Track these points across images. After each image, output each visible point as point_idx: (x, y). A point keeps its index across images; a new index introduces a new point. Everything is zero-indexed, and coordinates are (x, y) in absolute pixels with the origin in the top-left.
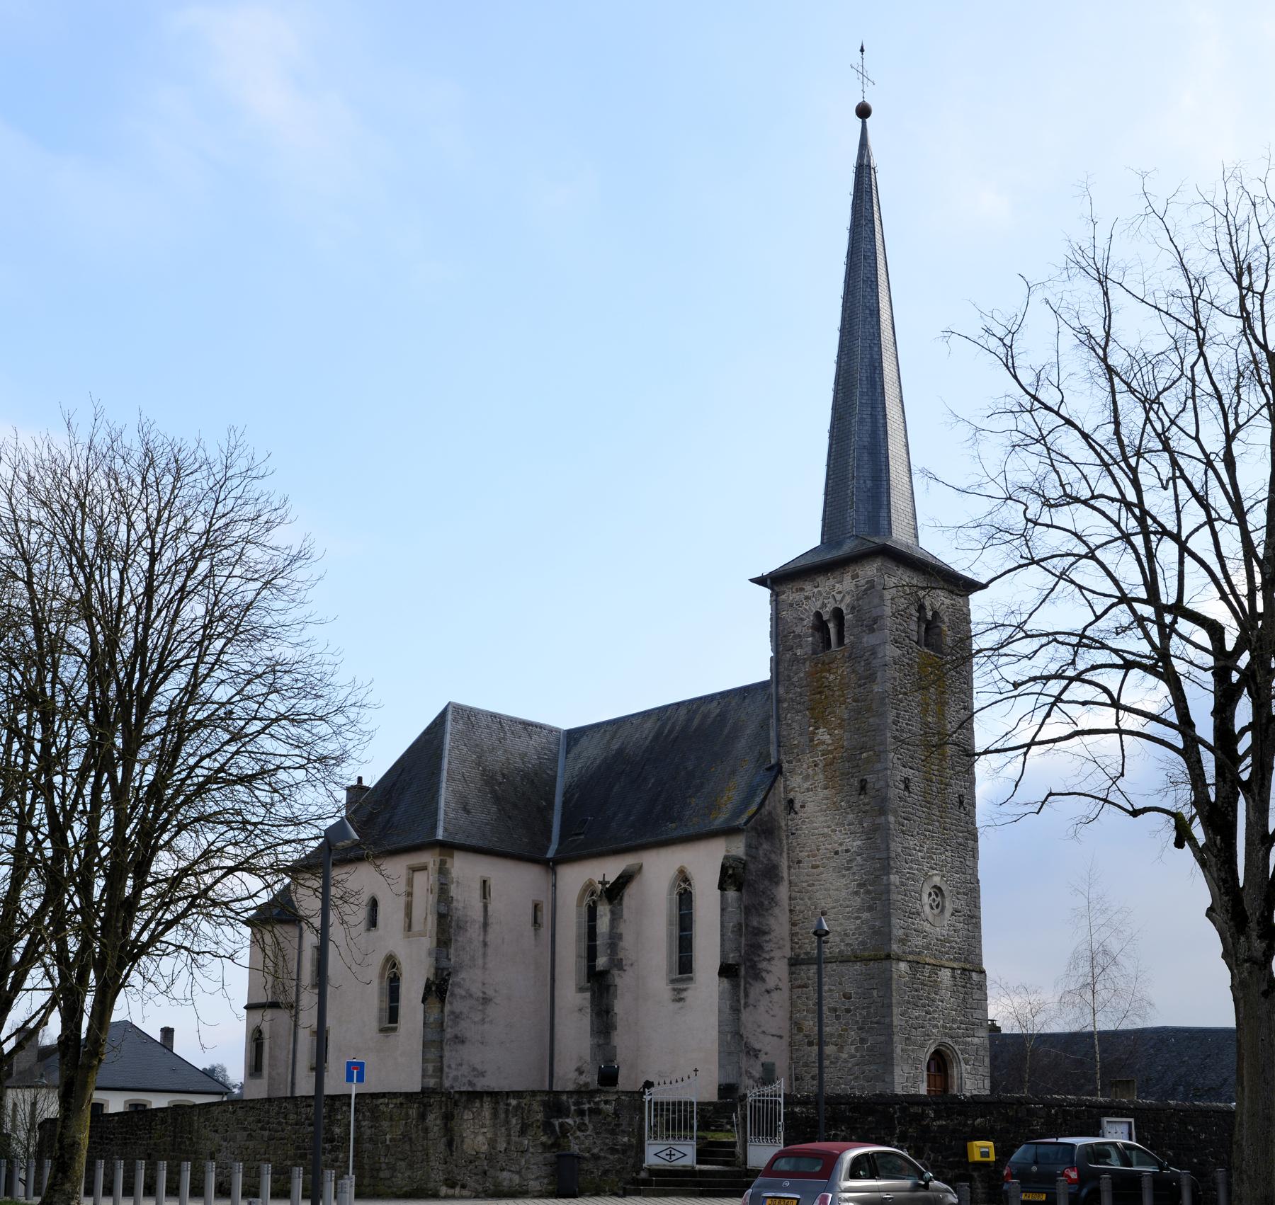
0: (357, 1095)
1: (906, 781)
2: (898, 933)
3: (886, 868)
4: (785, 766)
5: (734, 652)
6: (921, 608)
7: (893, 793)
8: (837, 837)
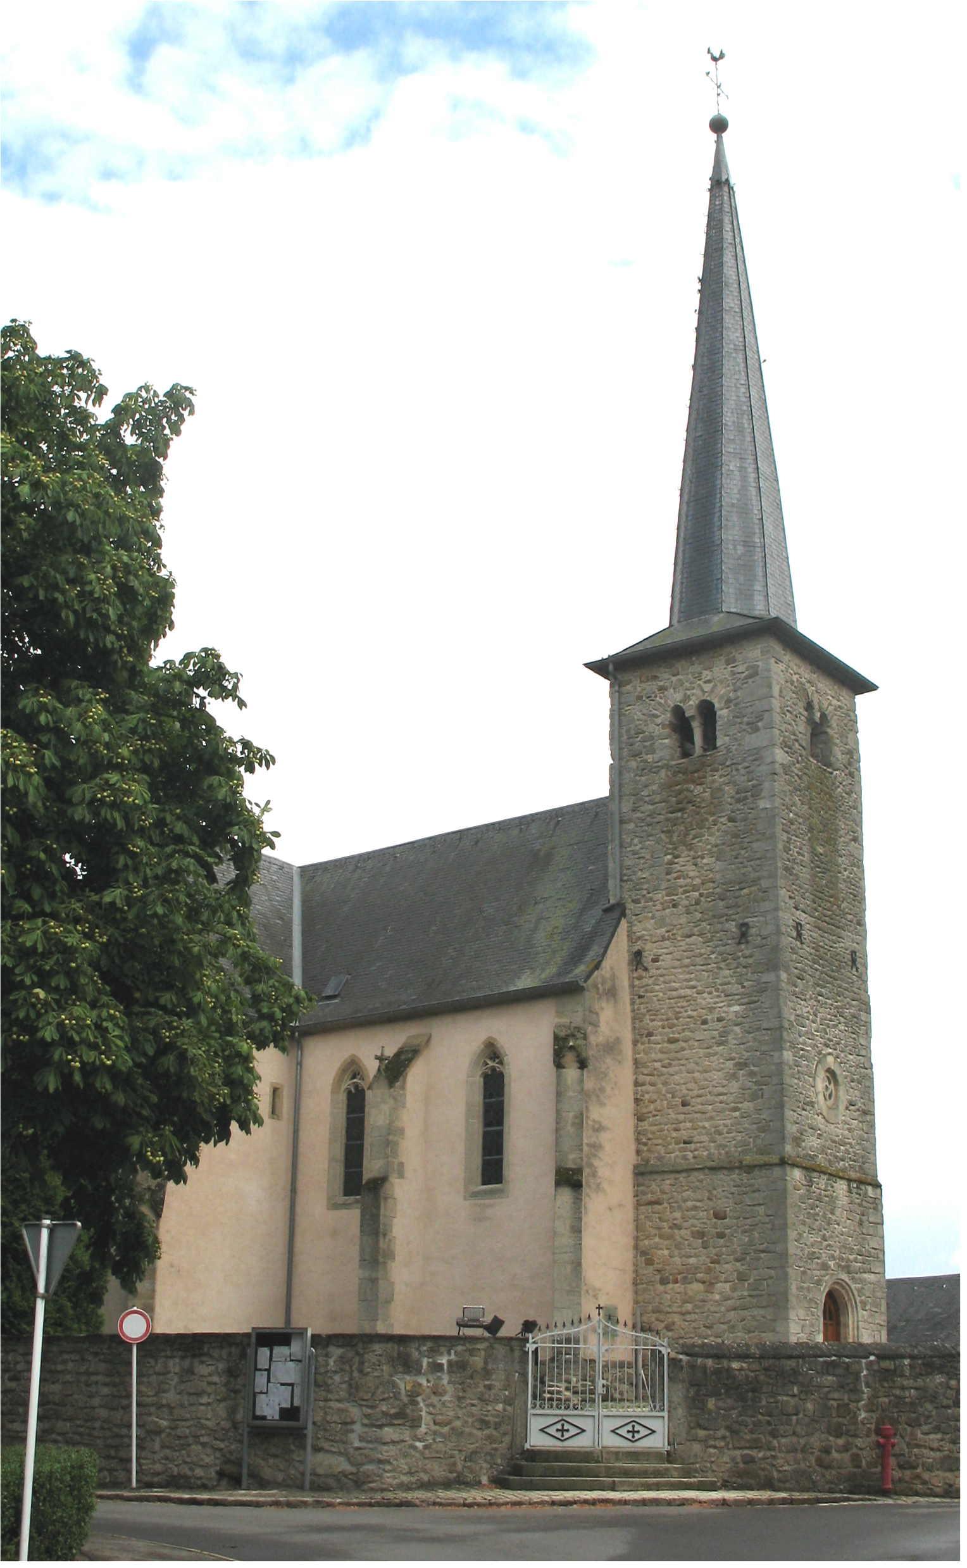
0: (312, 1335)
1: (798, 926)
2: (791, 1129)
3: (778, 1044)
4: (630, 906)
5: (563, 757)
6: (809, 707)
7: (787, 941)
8: (707, 999)
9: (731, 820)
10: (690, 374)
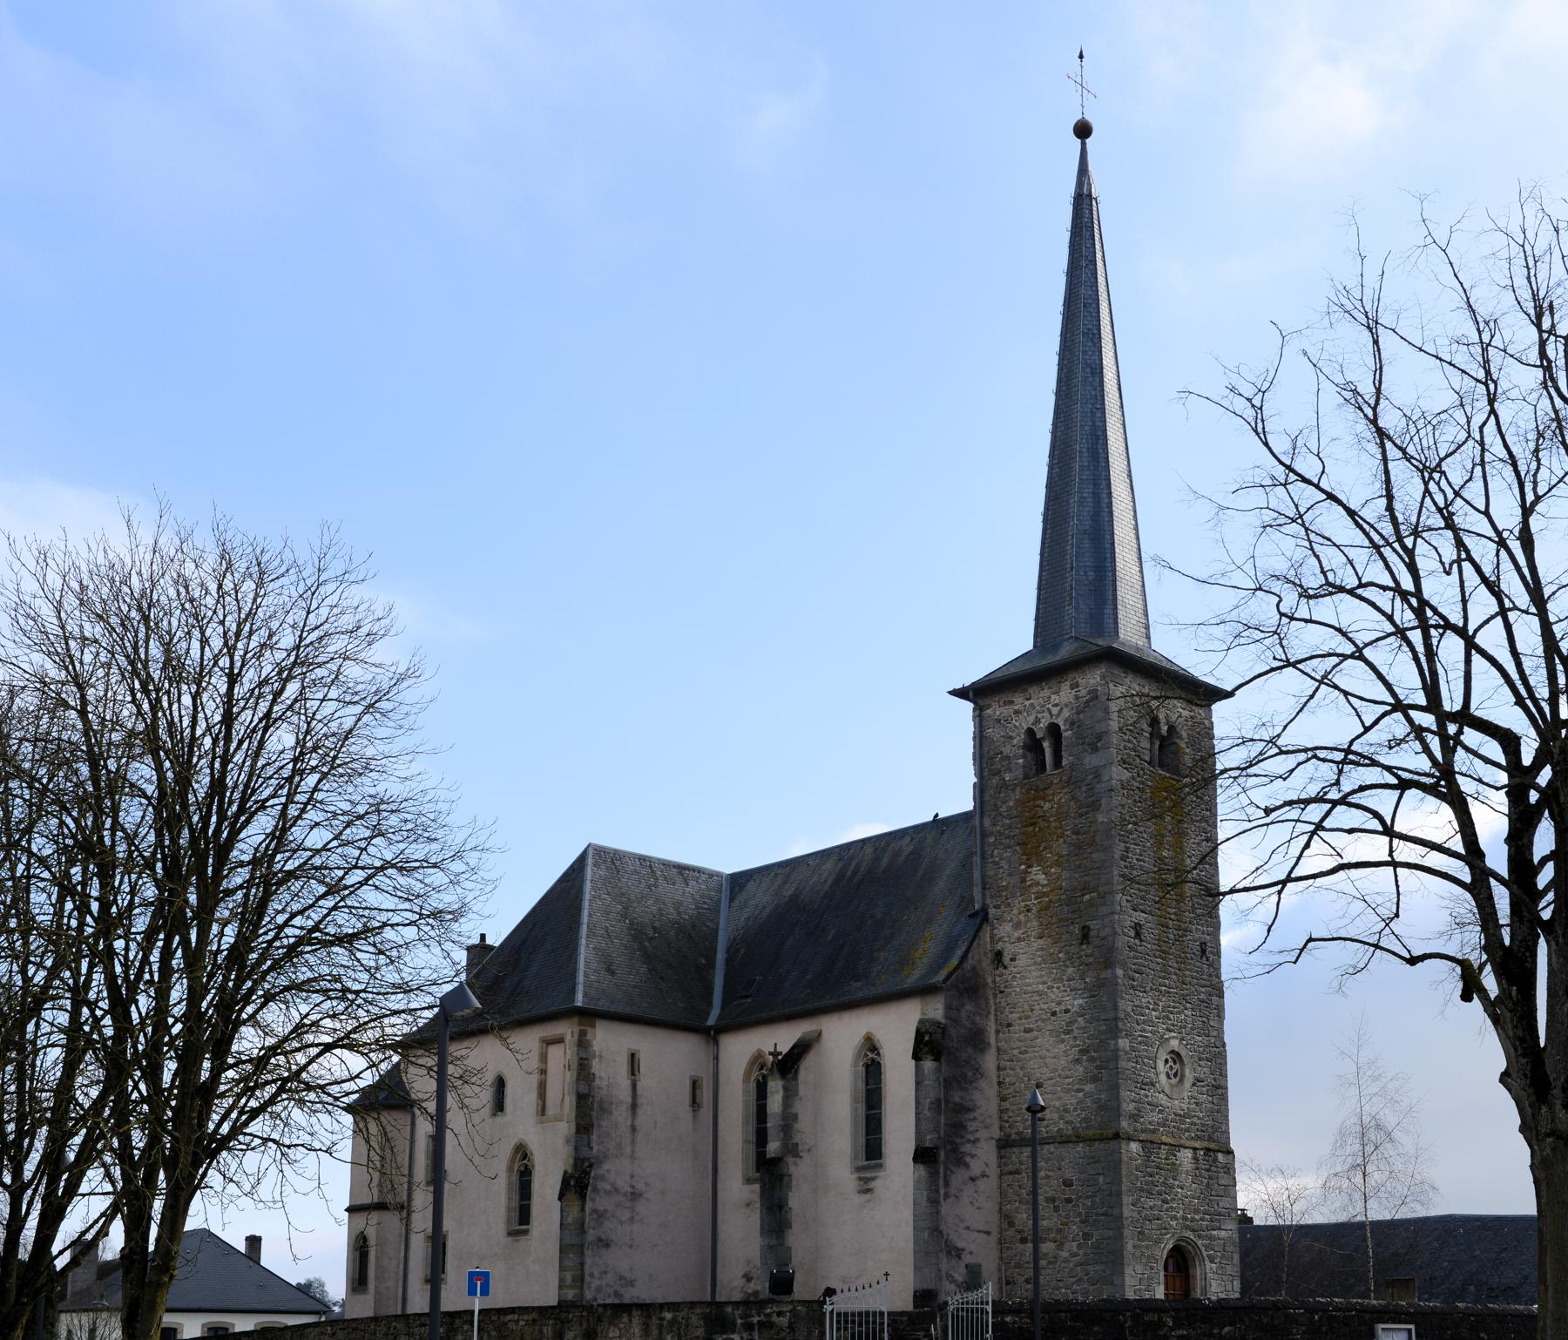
1: (1137, 928)
5: (929, 775)
6: (1154, 722)
9: (1077, 833)
10: (1053, 398)
